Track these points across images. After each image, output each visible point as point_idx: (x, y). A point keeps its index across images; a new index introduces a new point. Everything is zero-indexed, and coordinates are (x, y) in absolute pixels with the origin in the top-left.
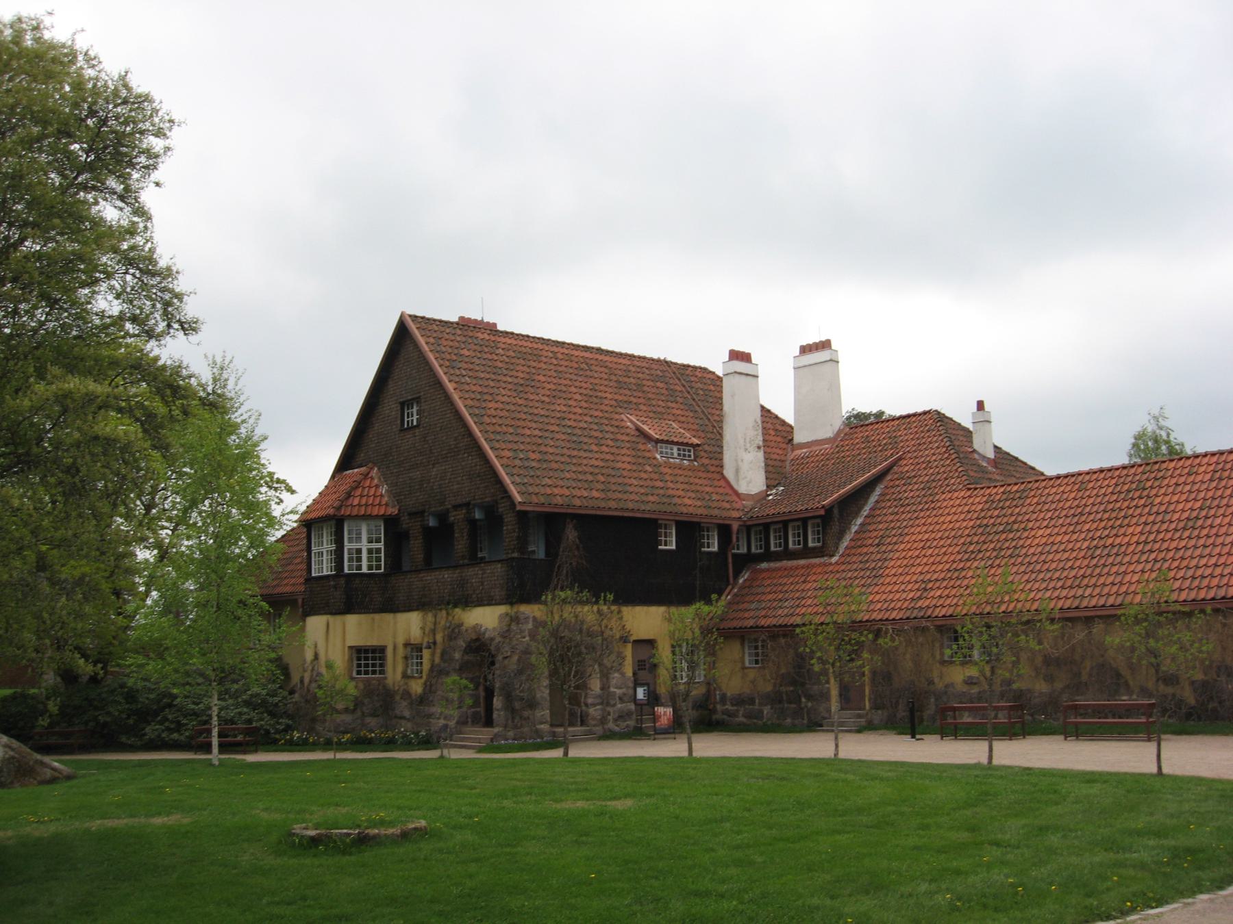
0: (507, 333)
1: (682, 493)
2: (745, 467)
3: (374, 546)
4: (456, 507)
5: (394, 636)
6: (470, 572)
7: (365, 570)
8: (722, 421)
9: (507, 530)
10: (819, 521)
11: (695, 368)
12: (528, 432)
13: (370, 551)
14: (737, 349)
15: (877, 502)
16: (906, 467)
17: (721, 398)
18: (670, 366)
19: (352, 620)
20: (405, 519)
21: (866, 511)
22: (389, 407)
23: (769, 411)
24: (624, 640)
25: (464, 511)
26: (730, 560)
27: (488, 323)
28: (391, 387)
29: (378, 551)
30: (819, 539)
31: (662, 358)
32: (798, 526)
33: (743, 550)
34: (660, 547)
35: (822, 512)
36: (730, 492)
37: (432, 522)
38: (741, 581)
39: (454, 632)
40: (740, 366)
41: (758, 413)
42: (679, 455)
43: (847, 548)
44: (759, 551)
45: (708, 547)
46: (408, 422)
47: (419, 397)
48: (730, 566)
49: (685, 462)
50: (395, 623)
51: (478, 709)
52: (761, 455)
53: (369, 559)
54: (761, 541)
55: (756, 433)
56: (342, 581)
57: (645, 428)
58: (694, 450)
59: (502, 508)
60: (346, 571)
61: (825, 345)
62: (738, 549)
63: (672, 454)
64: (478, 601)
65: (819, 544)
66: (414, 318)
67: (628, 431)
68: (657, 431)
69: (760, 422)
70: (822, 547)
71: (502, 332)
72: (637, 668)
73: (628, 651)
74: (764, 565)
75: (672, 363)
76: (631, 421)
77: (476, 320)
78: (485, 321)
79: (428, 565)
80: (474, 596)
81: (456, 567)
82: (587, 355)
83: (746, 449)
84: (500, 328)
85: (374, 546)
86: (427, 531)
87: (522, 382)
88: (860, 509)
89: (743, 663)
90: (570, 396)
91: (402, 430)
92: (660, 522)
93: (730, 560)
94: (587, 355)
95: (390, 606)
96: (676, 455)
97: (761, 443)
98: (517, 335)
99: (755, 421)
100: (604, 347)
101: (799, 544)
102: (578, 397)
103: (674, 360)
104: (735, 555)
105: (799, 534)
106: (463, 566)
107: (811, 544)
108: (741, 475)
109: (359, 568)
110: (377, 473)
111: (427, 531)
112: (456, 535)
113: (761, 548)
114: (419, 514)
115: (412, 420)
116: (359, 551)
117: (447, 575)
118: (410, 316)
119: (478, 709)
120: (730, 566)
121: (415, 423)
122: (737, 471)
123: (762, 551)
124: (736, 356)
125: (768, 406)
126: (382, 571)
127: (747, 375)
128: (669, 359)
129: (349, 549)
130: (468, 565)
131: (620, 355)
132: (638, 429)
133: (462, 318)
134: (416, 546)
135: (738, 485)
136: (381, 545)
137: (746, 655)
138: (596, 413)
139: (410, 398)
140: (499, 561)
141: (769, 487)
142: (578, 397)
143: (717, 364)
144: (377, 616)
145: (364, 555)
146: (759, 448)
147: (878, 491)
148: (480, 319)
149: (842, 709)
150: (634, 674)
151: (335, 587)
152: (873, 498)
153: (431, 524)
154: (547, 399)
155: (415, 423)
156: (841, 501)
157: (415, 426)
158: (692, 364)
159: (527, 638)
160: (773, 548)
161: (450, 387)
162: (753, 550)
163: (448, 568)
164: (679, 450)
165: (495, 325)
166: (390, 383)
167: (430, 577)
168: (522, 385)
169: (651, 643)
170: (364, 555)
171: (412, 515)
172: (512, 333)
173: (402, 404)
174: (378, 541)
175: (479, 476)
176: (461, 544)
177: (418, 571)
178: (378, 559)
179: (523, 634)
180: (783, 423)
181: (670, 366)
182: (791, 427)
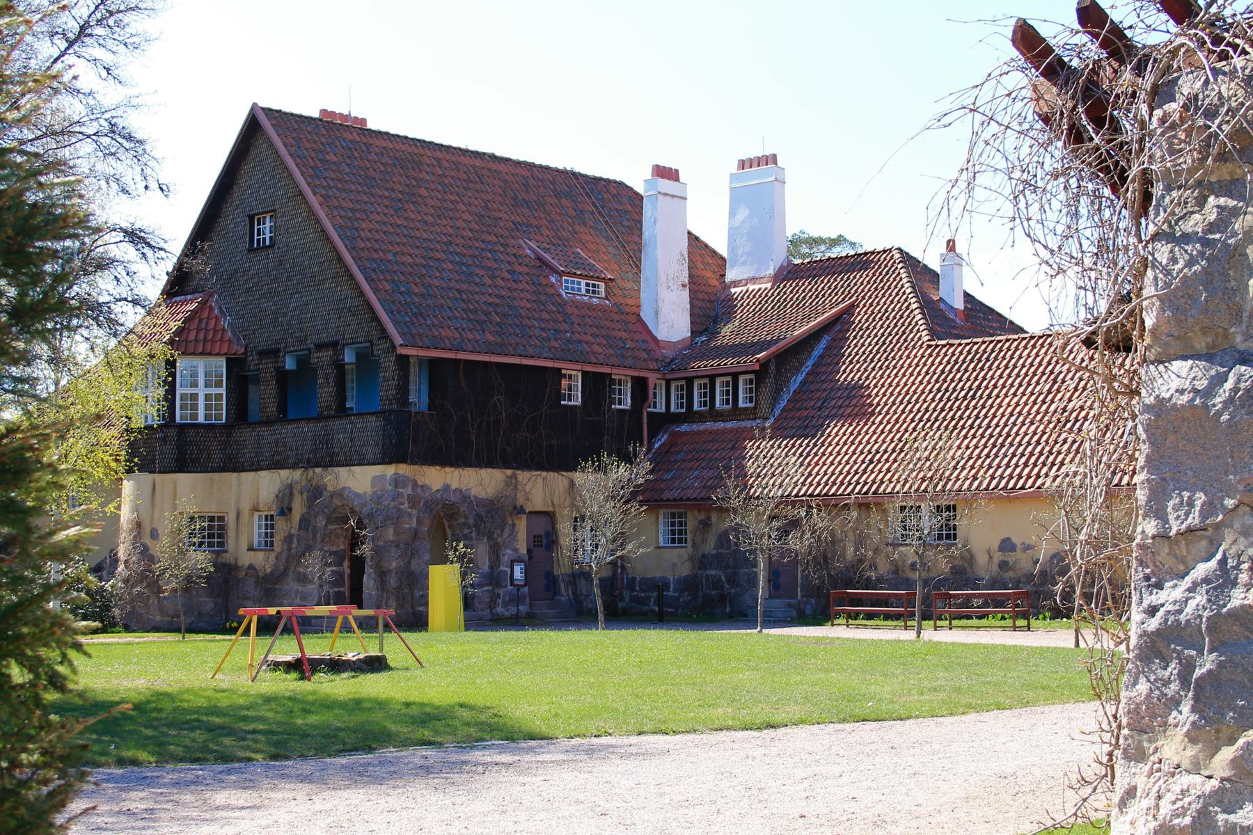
0: (380, 132)
1: (590, 339)
2: (665, 308)
3: (213, 391)
4: (320, 347)
5: (238, 501)
6: (336, 425)
7: (201, 419)
8: (640, 251)
9: (384, 377)
10: (752, 376)
11: (608, 181)
12: (410, 260)
13: (208, 397)
14: (662, 164)
15: (821, 357)
16: (859, 317)
17: (640, 222)
18: (577, 179)
19: (184, 479)
20: (253, 359)
21: (807, 368)
22: (233, 219)
23: (697, 238)
24: (521, 510)
25: (330, 353)
26: (645, 420)
27: (356, 118)
28: (236, 195)
29: (218, 397)
30: (751, 398)
31: (569, 169)
32: (728, 382)
33: (661, 408)
34: (562, 402)
35: (757, 367)
36: (648, 338)
37: (290, 364)
38: (657, 446)
39: (315, 492)
40: (665, 185)
41: (684, 242)
42: (587, 291)
43: (783, 410)
44: (679, 410)
45: (570, 400)
46: (259, 240)
47: (274, 211)
48: (645, 427)
49: (595, 300)
50: (239, 485)
51: (342, 589)
52: (686, 294)
53: (207, 407)
54: (259, 230)
55: (681, 267)
56: (173, 433)
57: (547, 257)
58: (606, 287)
59: (380, 348)
60: (178, 420)
61: (773, 159)
62: (655, 407)
63: (579, 290)
64: (346, 460)
65: (752, 405)
66: (268, 112)
67: (527, 260)
68: (562, 261)
69: (686, 256)
70: (755, 408)
71: (374, 132)
72: (532, 546)
73: (522, 524)
74: (685, 427)
75: (580, 174)
76: (530, 248)
77: (341, 114)
78: (353, 115)
79: (283, 416)
80: (341, 455)
81: (318, 419)
82: (478, 163)
83: (669, 287)
84: (371, 125)
85: (213, 391)
86: (283, 377)
87: (400, 196)
88: (801, 364)
89: (657, 542)
90: (458, 215)
91: (251, 249)
92: (563, 371)
93: (645, 420)
94: (478, 163)
95: (233, 465)
96: (583, 292)
97: (687, 280)
98: (393, 135)
99: (681, 253)
100: (498, 154)
101: (682, 407)
102: (466, 216)
103: (583, 172)
104: (649, 414)
105: (728, 392)
106: (329, 417)
107: (741, 404)
108: (662, 318)
109: (195, 416)
110: (217, 301)
111: (283, 377)
112: (320, 381)
113: (682, 407)
114: (272, 353)
115: (264, 239)
116: (194, 397)
117: (306, 428)
118: (263, 109)
119: (342, 589)
120: (645, 427)
121: (268, 243)
122: (657, 313)
123: (684, 410)
124: (665, 173)
125: (696, 233)
126: (224, 421)
127: (673, 196)
128: (577, 170)
129: (182, 395)
130: (333, 417)
131: (518, 163)
132: (539, 259)
133: (324, 112)
134: (264, 397)
135: (657, 330)
136: (223, 391)
137: (661, 526)
138: (489, 238)
139: (261, 211)
140: (373, 414)
141: (694, 333)
142: (466, 216)
143: (637, 180)
144: (217, 476)
145: (201, 403)
146: (684, 286)
147: (823, 343)
148: (346, 113)
149: (770, 597)
150: (529, 551)
151: (164, 440)
152: (817, 353)
153: (287, 367)
154: (430, 219)
155: (268, 243)
156: (779, 354)
157: (268, 247)
158: (605, 176)
159: (406, 505)
160: (696, 407)
161: (314, 201)
162: (673, 409)
163: (309, 420)
164: (587, 285)
165: (364, 121)
166: (236, 190)
167: (286, 431)
168: (400, 200)
169: (550, 516)
170: (201, 403)
171: (262, 354)
172: (387, 134)
173: (251, 218)
174: (218, 385)
175: (350, 311)
176: (325, 394)
177: (269, 423)
178: (218, 407)
179: (402, 500)
180: (714, 253)
181: (577, 179)
182: (723, 259)
